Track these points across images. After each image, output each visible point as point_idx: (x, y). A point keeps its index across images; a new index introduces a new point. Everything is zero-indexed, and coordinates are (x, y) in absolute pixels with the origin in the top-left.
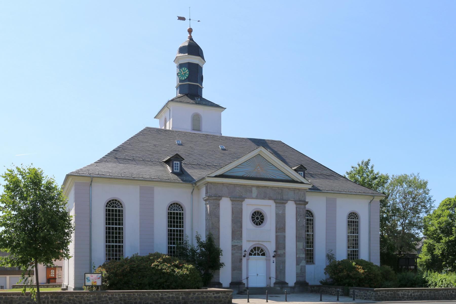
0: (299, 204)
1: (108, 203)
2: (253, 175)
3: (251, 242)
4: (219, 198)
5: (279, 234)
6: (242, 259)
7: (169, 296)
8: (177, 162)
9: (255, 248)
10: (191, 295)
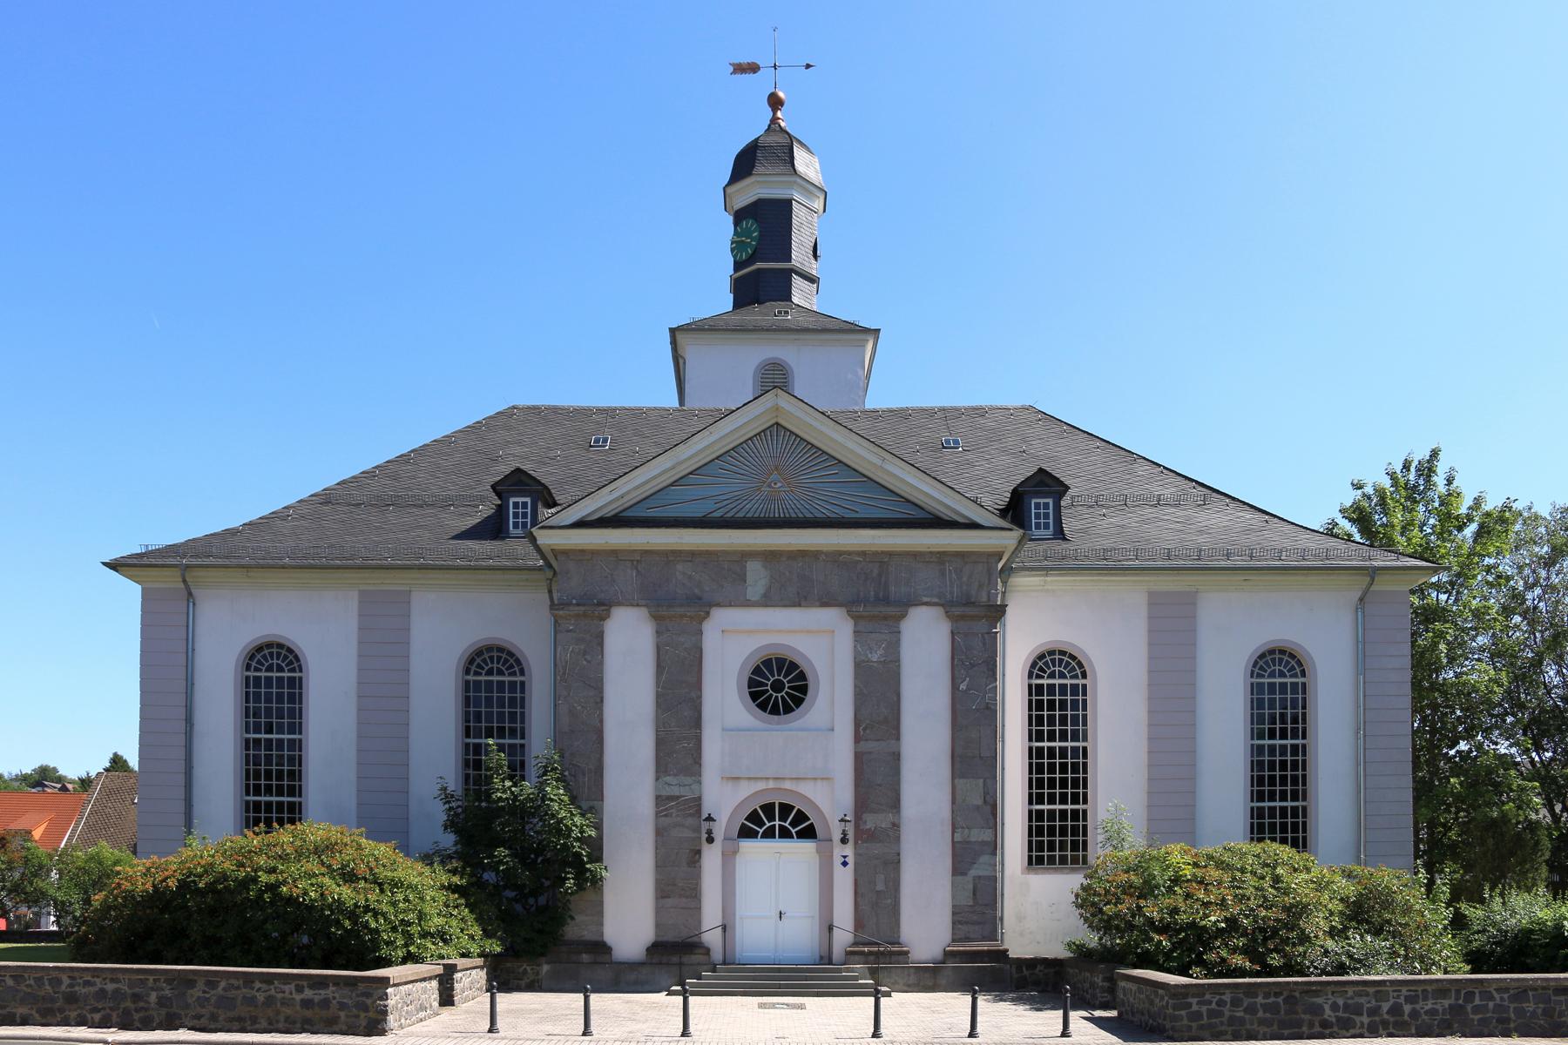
0: (962, 617)
1: (1034, 665)
2: (752, 509)
3: (744, 783)
4: (597, 608)
5: (864, 746)
6: (699, 852)
7: (102, 991)
8: (1042, 501)
9: (768, 809)
10: (196, 992)
